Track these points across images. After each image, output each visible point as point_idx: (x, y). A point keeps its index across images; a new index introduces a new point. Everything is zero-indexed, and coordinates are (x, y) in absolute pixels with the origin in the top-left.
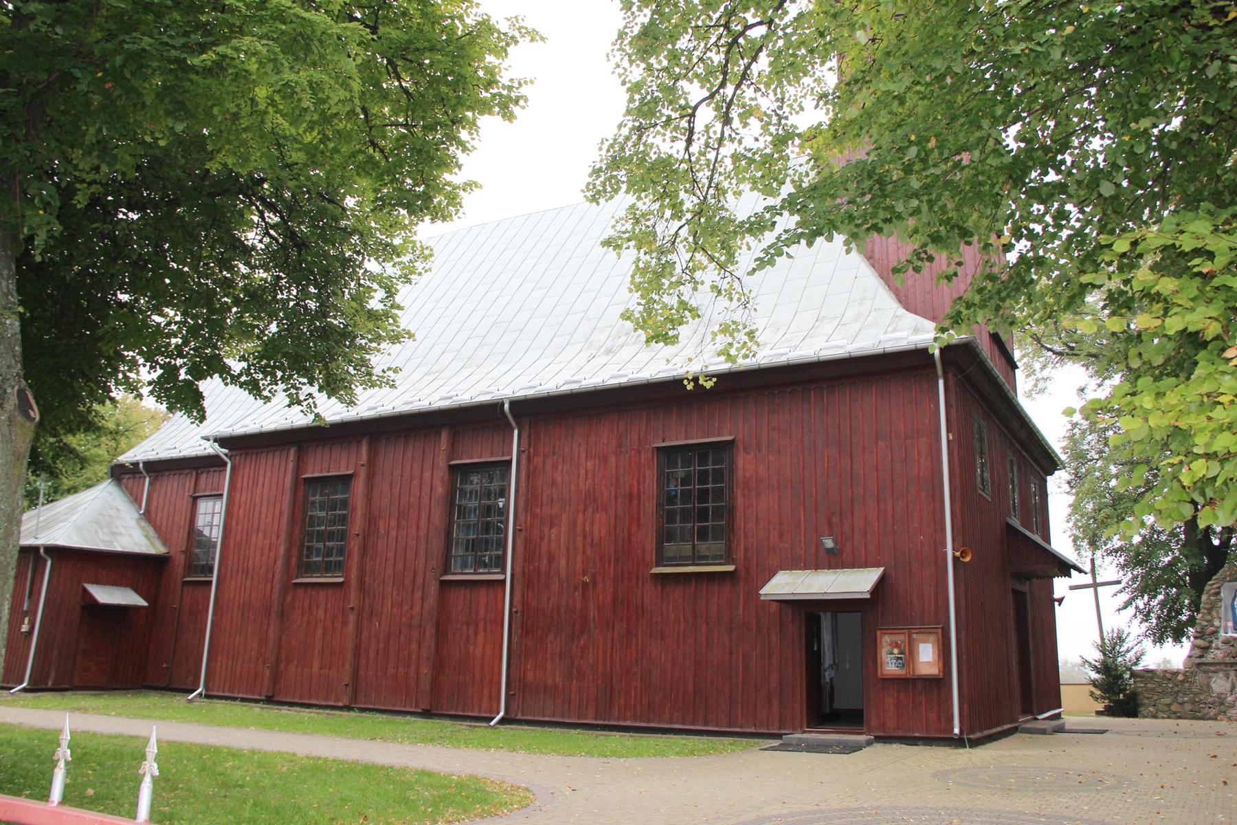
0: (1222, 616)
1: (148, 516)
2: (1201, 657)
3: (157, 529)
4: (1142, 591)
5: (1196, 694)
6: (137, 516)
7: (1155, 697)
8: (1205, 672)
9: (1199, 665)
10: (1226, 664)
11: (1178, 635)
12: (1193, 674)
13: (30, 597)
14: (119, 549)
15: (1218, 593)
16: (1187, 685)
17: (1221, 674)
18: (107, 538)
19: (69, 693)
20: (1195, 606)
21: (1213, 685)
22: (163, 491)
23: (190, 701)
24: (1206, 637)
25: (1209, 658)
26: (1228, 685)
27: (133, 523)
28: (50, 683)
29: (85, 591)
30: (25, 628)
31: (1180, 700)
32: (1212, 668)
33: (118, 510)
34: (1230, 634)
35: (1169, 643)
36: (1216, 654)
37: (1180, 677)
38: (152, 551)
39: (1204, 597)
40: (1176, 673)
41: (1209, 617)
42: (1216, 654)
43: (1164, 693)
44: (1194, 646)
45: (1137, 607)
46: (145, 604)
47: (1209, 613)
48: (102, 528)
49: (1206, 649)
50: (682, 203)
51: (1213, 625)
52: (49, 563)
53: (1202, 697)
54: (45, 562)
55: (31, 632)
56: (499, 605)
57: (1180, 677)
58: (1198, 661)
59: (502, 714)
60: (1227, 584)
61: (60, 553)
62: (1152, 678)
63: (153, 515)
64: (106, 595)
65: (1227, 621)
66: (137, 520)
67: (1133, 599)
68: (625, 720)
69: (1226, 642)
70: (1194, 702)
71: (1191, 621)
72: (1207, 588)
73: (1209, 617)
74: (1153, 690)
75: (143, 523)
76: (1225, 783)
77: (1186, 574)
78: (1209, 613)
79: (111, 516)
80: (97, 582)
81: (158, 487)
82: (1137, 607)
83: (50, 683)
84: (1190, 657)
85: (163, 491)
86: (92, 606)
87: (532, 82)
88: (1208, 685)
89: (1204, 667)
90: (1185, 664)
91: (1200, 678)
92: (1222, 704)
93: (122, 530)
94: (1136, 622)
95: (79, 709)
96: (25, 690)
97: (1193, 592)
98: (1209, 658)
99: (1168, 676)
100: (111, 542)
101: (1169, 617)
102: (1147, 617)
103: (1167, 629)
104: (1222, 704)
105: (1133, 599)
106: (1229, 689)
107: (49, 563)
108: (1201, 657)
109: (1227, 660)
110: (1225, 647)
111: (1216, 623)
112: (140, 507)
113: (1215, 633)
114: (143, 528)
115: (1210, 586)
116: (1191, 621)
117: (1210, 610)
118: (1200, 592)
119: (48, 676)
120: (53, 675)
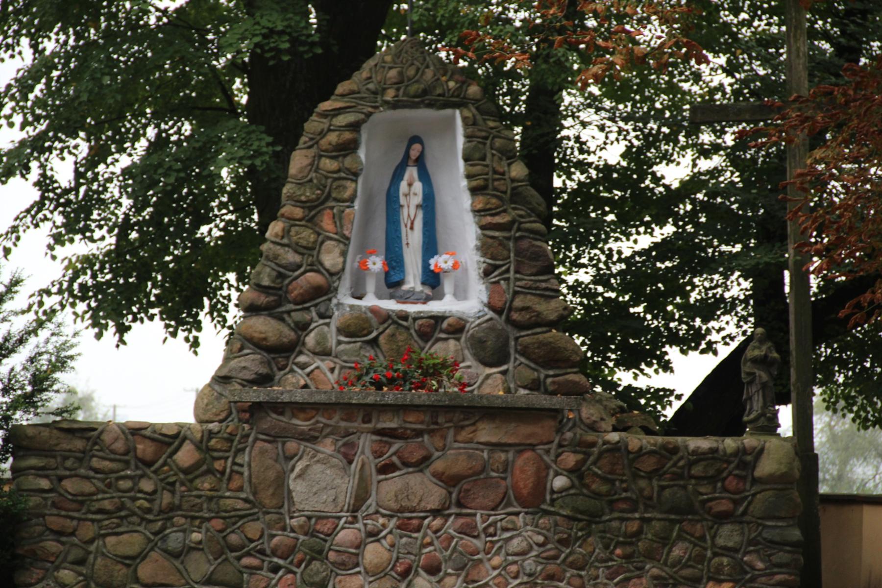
0: (353, 232)
2: (264, 380)
4: (64, 121)
5: (234, 518)
7: (88, 530)
8: (274, 437)
9: (256, 410)
10: (348, 409)
11: (182, 308)
12: (234, 444)
15: (349, 148)
16: (206, 484)
17: (327, 447)
20: (263, 191)
21: (297, 487)
24: (287, 305)
25: (291, 385)
26: (345, 486)
31: (175, 540)
32: (301, 424)
34: (370, 301)
35: (149, 331)
36: (318, 374)
37: (186, 456)
39: (298, 161)
40: (168, 439)
41: (307, 236)
42: (318, 374)
43: (121, 516)
44: (238, 343)
45: (45, 183)
47: (311, 221)
49: (281, 353)
50: (574, 295)
51: (316, 266)
53: (253, 529)
57: (186, 456)
58: (256, 395)
60: (384, 115)
62: (83, 457)
65: (366, 251)
67: (37, 146)
69: (356, 329)
70: (222, 549)
71: (239, 250)
72: (313, 125)
73: (307, 236)
74: (81, 500)
77: (235, 68)
78: (311, 221)
82: (45, 183)
84: (221, 379)
87: (185, 390)
88: (280, 482)
89: (272, 420)
90: (204, 403)
91: (255, 459)
92: (318, 554)
94: (37, 238)
97: (263, 141)
98: (291, 385)
99: (144, 449)
101: (157, 234)
102: (77, 221)
103: (143, 280)
104: (318, 554)
105: (37, 146)
106: (346, 499)
108: (264, 380)
109: (357, 394)
110: (348, 347)
111: (330, 258)
113: (322, 293)
115: (326, 120)
116: (239, 250)
117: (313, 209)
118: (288, 138)
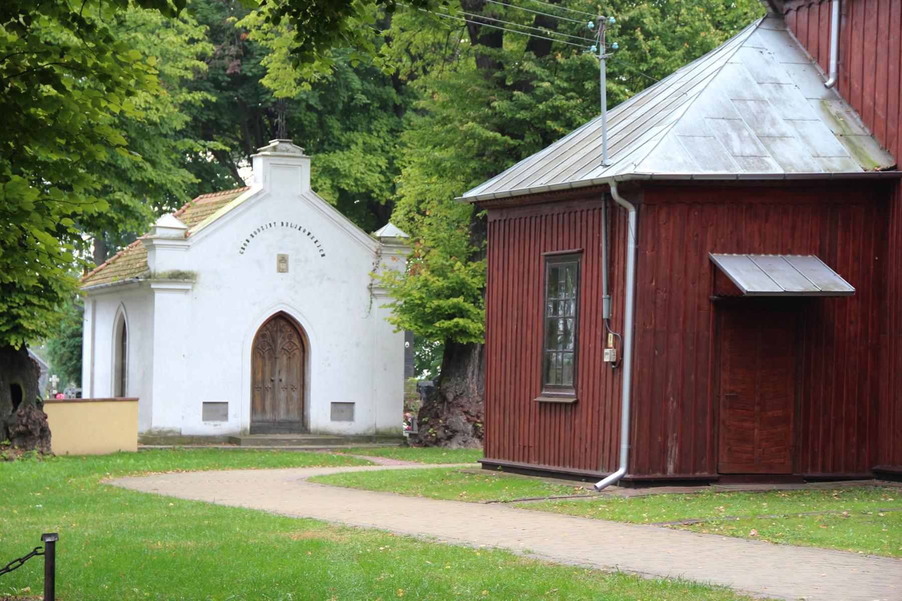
1: (845, 89)
3: (867, 116)
6: (822, 92)
13: (610, 290)
14: (775, 169)
18: (749, 150)
19: (706, 489)
22: (871, 23)
23: (600, 490)
27: (812, 110)
28: (671, 468)
29: (716, 270)
30: (609, 355)
33: (778, 85)
38: (857, 168)
46: (848, 288)
48: (738, 129)
52: (632, 215)
54: (626, 212)
55: (618, 364)
56: (823, 40)
59: (621, 471)
61: (649, 191)
63: (856, 86)
64: (755, 275)
66: (823, 102)
68: (654, 472)
75: (836, 107)
76: (283, 259)
79: (760, 101)
80: (740, 248)
81: (858, 18)
83: (671, 468)
85: (871, 23)
86: (732, 303)
93: (787, 129)
95: (690, 524)
96: (622, 482)
100: (759, 157)
107: (632, 215)
112: (827, 71)
114: (835, 119)
119: (664, 451)
120: (674, 451)
